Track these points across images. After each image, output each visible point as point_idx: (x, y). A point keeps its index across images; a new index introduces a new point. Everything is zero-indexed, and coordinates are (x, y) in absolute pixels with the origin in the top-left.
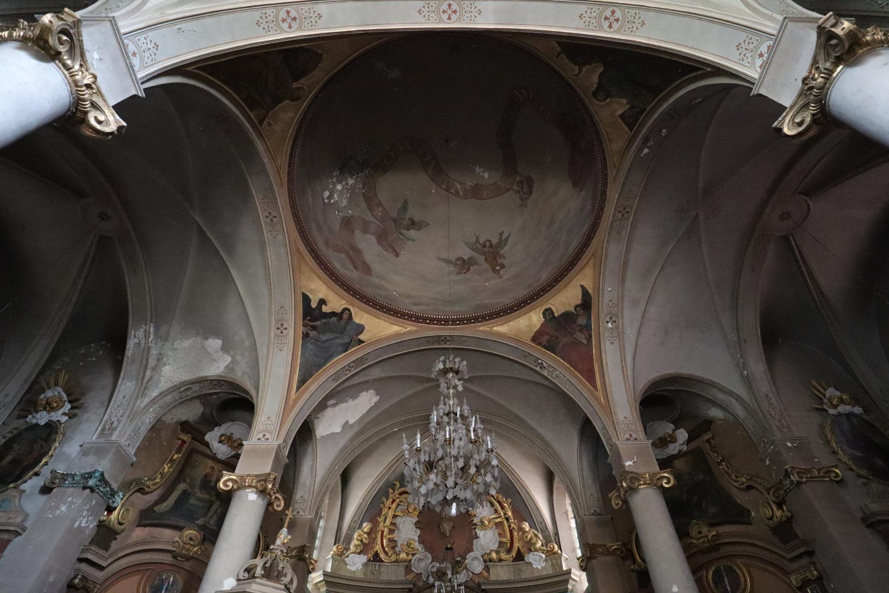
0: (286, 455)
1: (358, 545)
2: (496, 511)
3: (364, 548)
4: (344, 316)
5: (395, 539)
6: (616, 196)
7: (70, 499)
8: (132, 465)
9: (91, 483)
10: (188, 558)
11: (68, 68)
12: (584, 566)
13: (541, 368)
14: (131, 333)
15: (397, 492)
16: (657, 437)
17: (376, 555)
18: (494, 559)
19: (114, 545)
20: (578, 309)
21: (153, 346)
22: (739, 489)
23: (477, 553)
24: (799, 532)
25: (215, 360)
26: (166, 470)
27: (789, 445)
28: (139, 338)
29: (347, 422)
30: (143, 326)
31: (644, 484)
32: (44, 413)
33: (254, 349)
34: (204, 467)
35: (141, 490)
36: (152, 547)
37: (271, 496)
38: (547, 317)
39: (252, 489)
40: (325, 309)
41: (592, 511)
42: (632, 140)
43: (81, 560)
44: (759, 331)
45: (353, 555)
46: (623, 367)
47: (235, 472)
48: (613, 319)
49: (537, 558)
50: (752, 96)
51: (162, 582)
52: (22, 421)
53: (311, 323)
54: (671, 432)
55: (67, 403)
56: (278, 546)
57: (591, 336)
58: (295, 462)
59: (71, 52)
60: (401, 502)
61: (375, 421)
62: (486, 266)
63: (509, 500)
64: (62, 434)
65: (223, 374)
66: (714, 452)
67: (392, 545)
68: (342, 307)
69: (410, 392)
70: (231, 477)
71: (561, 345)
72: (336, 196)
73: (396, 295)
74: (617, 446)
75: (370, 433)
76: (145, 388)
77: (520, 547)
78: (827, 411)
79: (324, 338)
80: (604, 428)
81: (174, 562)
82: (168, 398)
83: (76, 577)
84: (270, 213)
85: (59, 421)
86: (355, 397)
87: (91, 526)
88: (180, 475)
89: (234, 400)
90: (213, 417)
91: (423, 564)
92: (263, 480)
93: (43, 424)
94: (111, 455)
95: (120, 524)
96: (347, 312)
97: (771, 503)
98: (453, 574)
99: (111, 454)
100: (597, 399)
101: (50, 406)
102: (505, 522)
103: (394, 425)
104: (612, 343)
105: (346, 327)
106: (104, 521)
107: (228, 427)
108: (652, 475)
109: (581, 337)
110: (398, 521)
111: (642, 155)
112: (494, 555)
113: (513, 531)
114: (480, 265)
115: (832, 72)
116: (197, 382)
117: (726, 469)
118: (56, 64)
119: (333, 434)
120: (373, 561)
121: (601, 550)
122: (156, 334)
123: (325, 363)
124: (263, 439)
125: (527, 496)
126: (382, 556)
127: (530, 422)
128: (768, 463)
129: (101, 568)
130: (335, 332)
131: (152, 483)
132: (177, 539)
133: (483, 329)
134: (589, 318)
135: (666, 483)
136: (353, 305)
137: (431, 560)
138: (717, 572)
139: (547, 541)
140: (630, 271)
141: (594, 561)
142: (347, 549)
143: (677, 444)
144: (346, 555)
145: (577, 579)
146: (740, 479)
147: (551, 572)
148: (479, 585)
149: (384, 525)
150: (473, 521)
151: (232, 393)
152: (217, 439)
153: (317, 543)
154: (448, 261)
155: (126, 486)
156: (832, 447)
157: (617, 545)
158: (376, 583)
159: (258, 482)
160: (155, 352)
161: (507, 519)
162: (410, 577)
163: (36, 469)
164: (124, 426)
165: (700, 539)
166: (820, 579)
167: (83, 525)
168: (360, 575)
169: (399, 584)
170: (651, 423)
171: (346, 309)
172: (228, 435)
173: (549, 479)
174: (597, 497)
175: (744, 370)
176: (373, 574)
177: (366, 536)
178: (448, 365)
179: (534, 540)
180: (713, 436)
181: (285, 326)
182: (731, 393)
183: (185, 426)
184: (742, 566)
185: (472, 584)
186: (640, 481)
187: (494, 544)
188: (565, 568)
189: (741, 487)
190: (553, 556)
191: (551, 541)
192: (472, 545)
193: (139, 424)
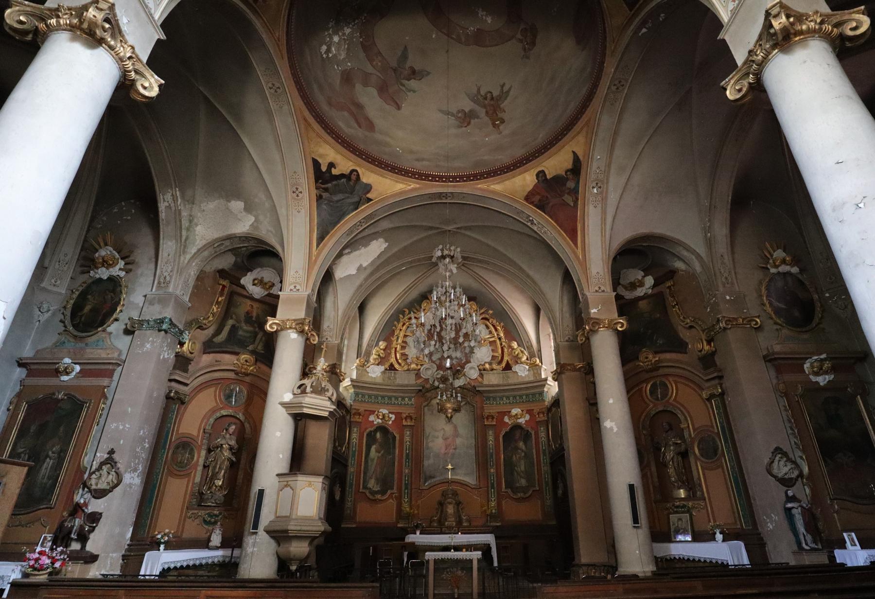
0: (315, 300)
1: (376, 359)
2: (491, 332)
3: (381, 361)
4: (352, 177)
6: (613, 70)
8: (189, 308)
9: (165, 326)
10: (247, 375)
11: (112, 48)
13: (532, 224)
14: (160, 198)
16: (628, 282)
17: (392, 365)
19: (191, 368)
20: (568, 173)
21: (182, 208)
22: (683, 327)
23: (474, 364)
24: (718, 363)
25: (240, 220)
26: (215, 310)
27: (728, 298)
28: (168, 202)
29: (361, 265)
30: (169, 190)
32: (104, 269)
33: (274, 208)
34: (245, 306)
36: (218, 368)
37: (307, 334)
38: (540, 179)
39: (293, 330)
40: (335, 172)
41: (567, 338)
42: (630, 20)
43: (170, 380)
44: (730, 198)
46: (602, 229)
47: (278, 316)
49: (522, 368)
50: (719, 40)
51: (232, 391)
52: (86, 276)
53: (323, 186)
54: (640, 278)
55: (120, 260)
56: (319, 371)
57: (577, 199)
59: (113, 36)
61: (387, 262)
62: (486, 119)
63: (502, 324)
65: (249, 232)
67: (404, 358)
69: (415, 239)
70: (275, 321)
71: (551, 204)
72: (333, 49)
75: (383, 272)
76: (185, 247)
78: (769, 269)
80: (579, 280)
82: (206, 253)
83: (170, 391)
84: (273, 85)
85: (118, 275)
86: (366, 245)
87: (172, 357)
88: (227, 312)
89: (262, 251)
91: (430, 372)
92: (300, 323)
93: (105, 278)
95: (191, 353)
96: (355, 173)
98: (454, 379)
99: (171, 306)
101: (107, 263)
103: (403, 265)
104: (595, 207)
105: (355, 187)
106: (179, 352)
107: (258, 272)
108: (611, 321)
109: (569, 199)
111: (640, 34)
112: (487, 366)
114: (481, 119)
115: (770, 53)
116: (228, 239)
117: (678, 311)
118: (103, 47)
119: (350, 275)
120: (390, 370)
121: (569, 368)
122: (183, 197)
123: (338, 222)
126: (397, 366)
129: (186, 385)
130: (346, 193)
131: (207, 321)
134: (578, 182)
135: (620, 327)
136: (359, 166)
137: (436, 369)
138: (654, 387)
139: (532, 355)
140: (620, 141)
141: (563, 376)
142: (368, 361)
143: (644, 288)
144: (367, 366)
146: (686, 320)
147: (532, 379)
148: (474, 387)
149: (397, 344)
152: (251, 282)
153: (344, 357)
154: (448, 113)
155: (189, 325)
158: (393, 386)
159: (297, 324)
161: (500, 339)
162: (419, 381)
163: (114, 316)
165: (646, 362)
166: (722, 394)
167: (166, 357)
168: (380, 381)
169: (411, 386)
170: (625, 270)
171: (353, 171)
172: (260, 278)
173: (537, 311)
176: (390, 379)
177: (382, 351)
178: (446, 252)
179: (521, 355)
181: (300, 190)
182: (693, 252)
183: (222, 273)
185: (469, 386)
186: (600, 325)
187: (488, 357)
188: (543, 376)
190: (535, 368)
191: (535, 356)
193: (187, 276)
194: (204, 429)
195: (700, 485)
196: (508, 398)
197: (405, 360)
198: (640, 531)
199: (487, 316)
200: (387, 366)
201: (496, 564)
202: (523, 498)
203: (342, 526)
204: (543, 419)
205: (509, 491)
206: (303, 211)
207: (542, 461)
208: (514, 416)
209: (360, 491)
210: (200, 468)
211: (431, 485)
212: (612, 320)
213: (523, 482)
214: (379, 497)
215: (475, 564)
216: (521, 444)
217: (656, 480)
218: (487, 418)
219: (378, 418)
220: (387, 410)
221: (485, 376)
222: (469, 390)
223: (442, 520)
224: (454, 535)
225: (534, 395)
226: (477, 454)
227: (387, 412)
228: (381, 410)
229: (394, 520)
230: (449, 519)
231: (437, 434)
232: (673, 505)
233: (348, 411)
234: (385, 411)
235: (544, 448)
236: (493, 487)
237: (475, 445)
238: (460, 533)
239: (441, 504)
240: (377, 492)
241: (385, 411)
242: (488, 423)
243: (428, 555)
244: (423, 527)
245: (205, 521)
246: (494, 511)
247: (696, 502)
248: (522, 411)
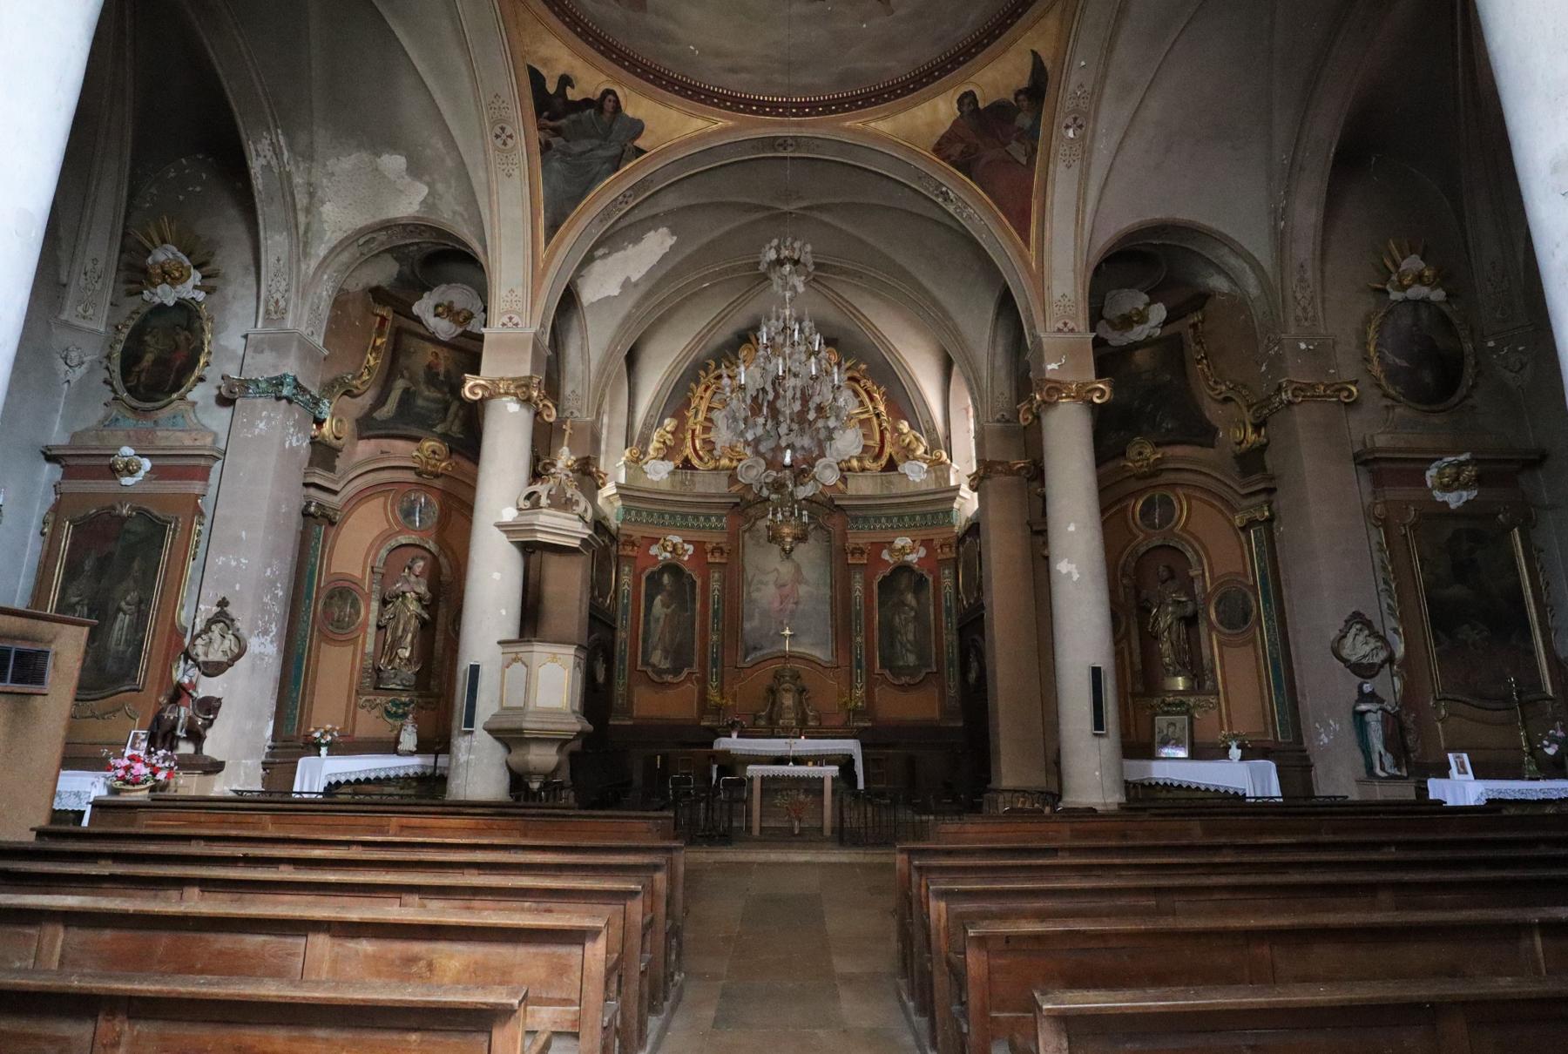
0: (547, 344)
1: (661, 449)
2: (862, 403)
3: (668, 453)
4: (605, 105)
7: (264, 413)
8: (325, 359)
9: (286, 391)
10: (437, 476)
13: (945, 200)
14: (250, 148)
16: (1119, 314)
17: (687, 461)
20: (1021, 97)
21: (293, 169)
23: (830, 459)
26: (372, 363)
27: (1303, 346)
28: (265, 157)
29: (628, 279)
31: (1067, 397)
35: (348, 393)
36: (382, 465)
37: (537, 405)
40: (573, 94)
41: (998, 416)
43: (306, 485)
47: (482, 373)
48: (1079, 122)
49: (917, 469)
51: (413, 503)
52: (137, 299)
53: (551, 124)
54: (1141, 308)
57: (1035, 150)
60: (718, 388)
63: (883, 389)
64: (208, 319)
66: (1197, 344)
67: (709, 447)
68: (603, 88)
70: (478, 381)
71: (983, 161)
73: (693, 52)
74: (1041, 339)
76: (306, 244)
78: (1388, 293)
79: (576, 148)
80: (1028, 309)
81: (420, 480)
82: (345, 257)
85: (193, 298)
86: (637, 240)
87: (304, 444)
90: (416, 276)
91: (753, 473)
94: (294, 349)
96: (611, 97)
97: (1247, 423)
98: (795, 486)
100: (1027, 264)
102: (875, 419)
104: (1069, 167)
105: (611, 126)
106: (316, 437)
107: (443, 292)
112: (855, 463)
117: (1206, 370)
124: (510, 325)
125: (912, 387)
126: (695, 462)
127: (920, 278)
128: (1264, 368)
129: (335, 493)
132: (415, 453)
133: (852, 123)
136: (620, 83)
139: (934, 445)
141: (988, 482)
142: (645, 453)
143: (1146, 326)
146: (1219, 387)
148: (831, 500)
149: (695, 422)
151: (437, 244)
152: (432, 310)
153: (603, 447)
155: (329, 388)
156: (1367, 352)
159: (517, 387)
160: (300, 181)
161: (878, 415)
162: (735, 488)
163: (197, 373)
164: (296, 306)
165: (1138, 461)
167: (294, 445)
168: (666, 487)
170: (1114, 292)
171: (608, 92)
172: (446, 303)
175: (1282, 219)
177: (669, 436)
178: (785, 253)
179: (914, 445)
180: (1203, 318)
183: (377, 294)
184: (1182, 498)
188: (953, 483)
189: (1216, 397)
190: (938, 467)
191: (940, 448)
194: (372, 568)
195: (1213, 671)
196: (889, 519)
198: (1104, 741)
199: (857, 375)
201: (861, 786)
202: (909, 685)
205: (887, 672)
206: (517, 172)
209: (638, 668)
210: (372, 630)
212: (1084, 384)
213: (911, 659)
214: (669, 678)
215: (828, 785)
216: (910, 598)
217: (1137, 659)
218: (853, 554)
219: (665, 550)
221: (849, 481)
223: (774, 717)
227: (680, 540)
232: (1163, 701)
233: (614, 538)
234: (677, 539)
236: (859, 666)
237: (831, 597)
239: (772, 691)
240: (667, 671)
241: (677, 539)
242: (854, 562)
244: (743, 727)
245: (388, 712)
246: (860, 704)
247: (1202, 698)
248: (914, 541)
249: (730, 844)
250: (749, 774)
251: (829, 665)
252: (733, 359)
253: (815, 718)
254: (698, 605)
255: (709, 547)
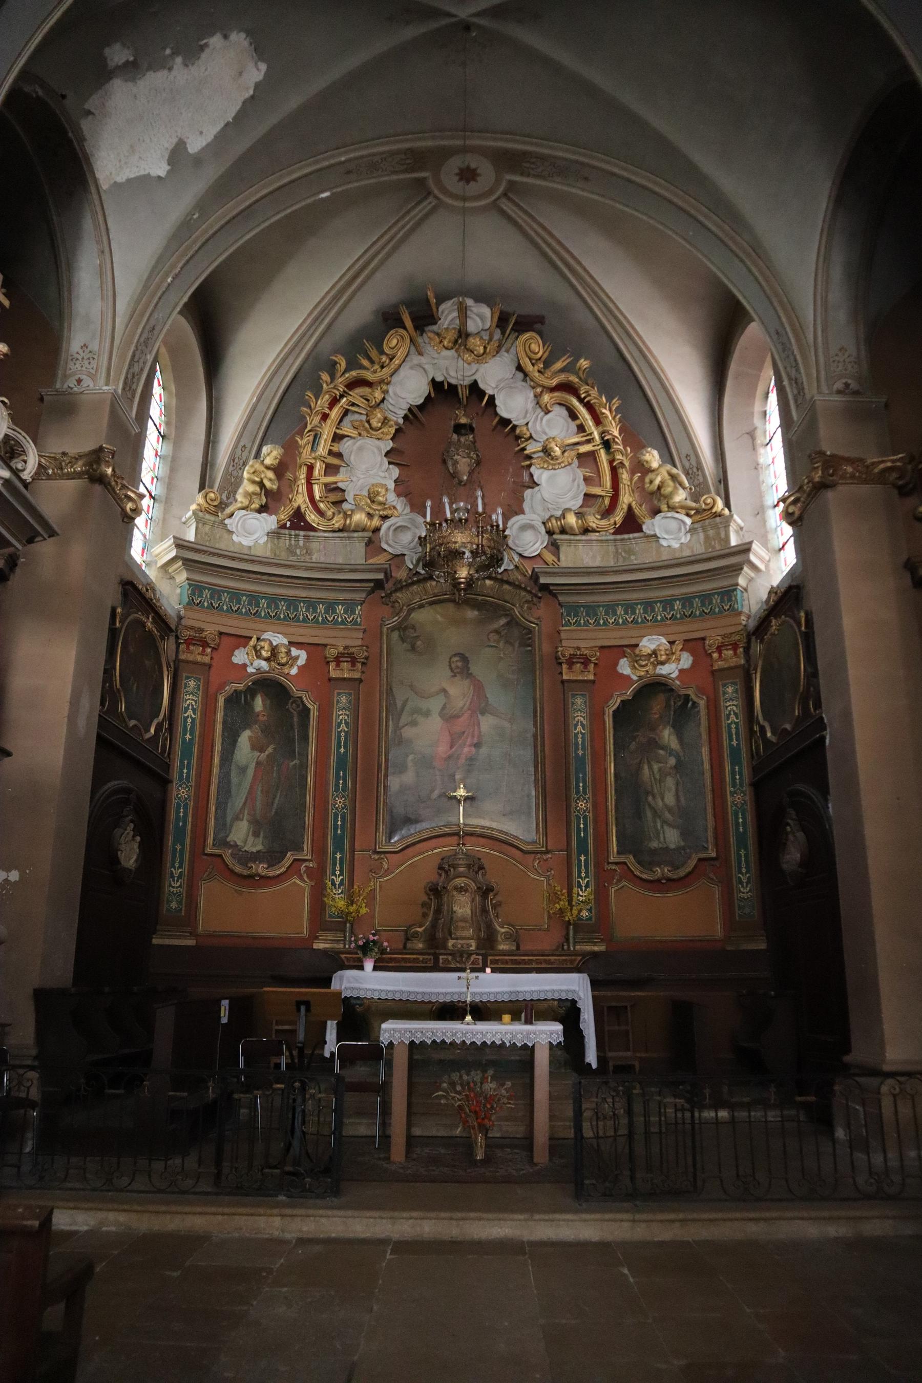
2: (581, 428)
5: (340, 485)
12: (797, 513)
15: (340, 380)
18: (572, 528)
41: (839, 385)
45: (244, 512)
58: (56, 258)
60: (353, 404)
63: (616, 402)
67: (333, 497)
77: (634, 505)
102: (602, 452)
110: (345, 447)
112: (572, 520)
113: (620, 470)
120: (290, 528)
126: (312, 517)
141: (830, 495)
145: (761, 566)
150: (524, 449)
157: (893, 461)
161: (607, 445)
169: (352, 571)
174: (855, 354)
177: (270, 474)
179: (667, 490)
187: (574, 498)
188: (734, 541)
192: (521, 500)
196: (630, 607)
197: (338, 503)
199: (573, 379)
200: (284, 514)
202: (669, 880)
203: (155, 941)
204: (734, 662)
205: (630, 860)
207: (728, 778)
208: (650, 655)
211: (411, 840)
213: (672, 837)
215: (542, 1060)
216: (667, 735)
218: (571, 664)
219: (259, 656)
220: (284, 634)
221: (563, 549)
222: (519, 587)
223: (440, 935)
224: (474, 975)
225: (706, 598)
226: (539, 762)
227: (285, 642)
228: (265, 636)
229: (305, 932)
230: (460, 933)
231: (424, 705)
234: (279, 639)
235: (735, 743)
237: (535, 736)
238: (488, 970)
239: (436, 892)
240: (255, 857)
241: (279, 639)
242: (572, 677)
243: (386, 1030)
244: (383, 951)
246: (585, 914)
248: (672, 643)
249: (336, 1192)
250: (384, 1039)
251: (529, 848)
252: (374, 353)
253: (508, 937)
254: (312, 748)
255: (332, 652)
